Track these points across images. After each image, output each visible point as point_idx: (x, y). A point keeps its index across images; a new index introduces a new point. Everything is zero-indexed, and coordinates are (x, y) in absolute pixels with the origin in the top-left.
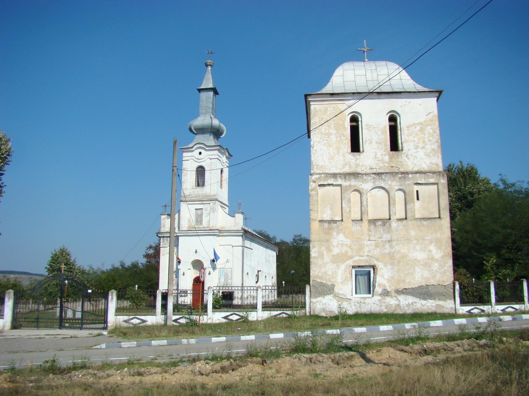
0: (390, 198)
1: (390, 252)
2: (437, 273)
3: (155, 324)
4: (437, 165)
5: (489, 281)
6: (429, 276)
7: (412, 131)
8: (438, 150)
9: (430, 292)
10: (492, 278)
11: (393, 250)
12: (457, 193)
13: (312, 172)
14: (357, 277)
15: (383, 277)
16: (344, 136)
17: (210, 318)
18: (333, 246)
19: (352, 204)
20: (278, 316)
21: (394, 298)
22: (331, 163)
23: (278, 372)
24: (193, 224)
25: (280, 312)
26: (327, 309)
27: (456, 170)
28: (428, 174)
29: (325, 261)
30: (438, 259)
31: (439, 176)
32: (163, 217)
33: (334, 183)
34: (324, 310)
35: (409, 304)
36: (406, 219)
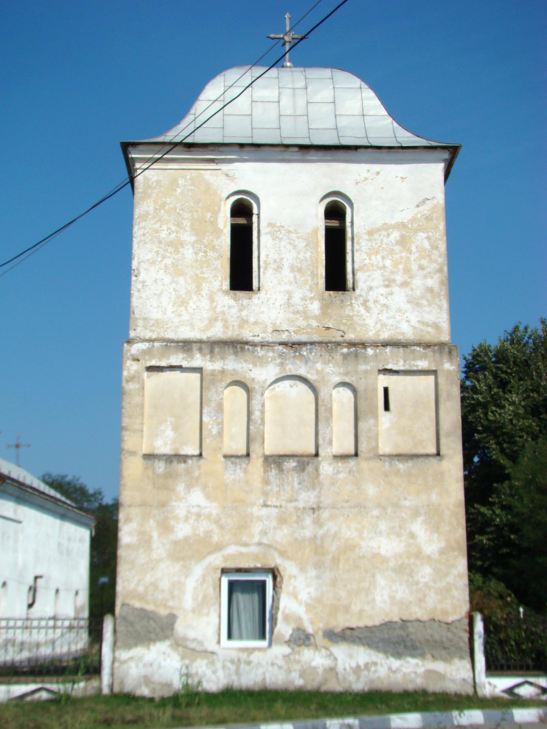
0: (320, 403)
1: (315, 536)
2: (430, 590)
4: (437, 327)
6: (410, 599)
7: (379, 242)
8: (441, 290)
9: (412, 640)
11: (321, 532)
12: (528, 397)
13: (132, 334)
14: (234, 596)
16: (214, 249)
18: (176, 518)
19: (226, 417)
21: (323, 652)
22: (180, 315)
25: (32, 687)
26: (156, 678)
27: (531, 341)
28: (413, 348)
29: (154, 555)
30: (433, 556)
31: (441, 353)
33: (185, 364)
34: (147, 680)
35: (358, 667)
36: (356, 455)
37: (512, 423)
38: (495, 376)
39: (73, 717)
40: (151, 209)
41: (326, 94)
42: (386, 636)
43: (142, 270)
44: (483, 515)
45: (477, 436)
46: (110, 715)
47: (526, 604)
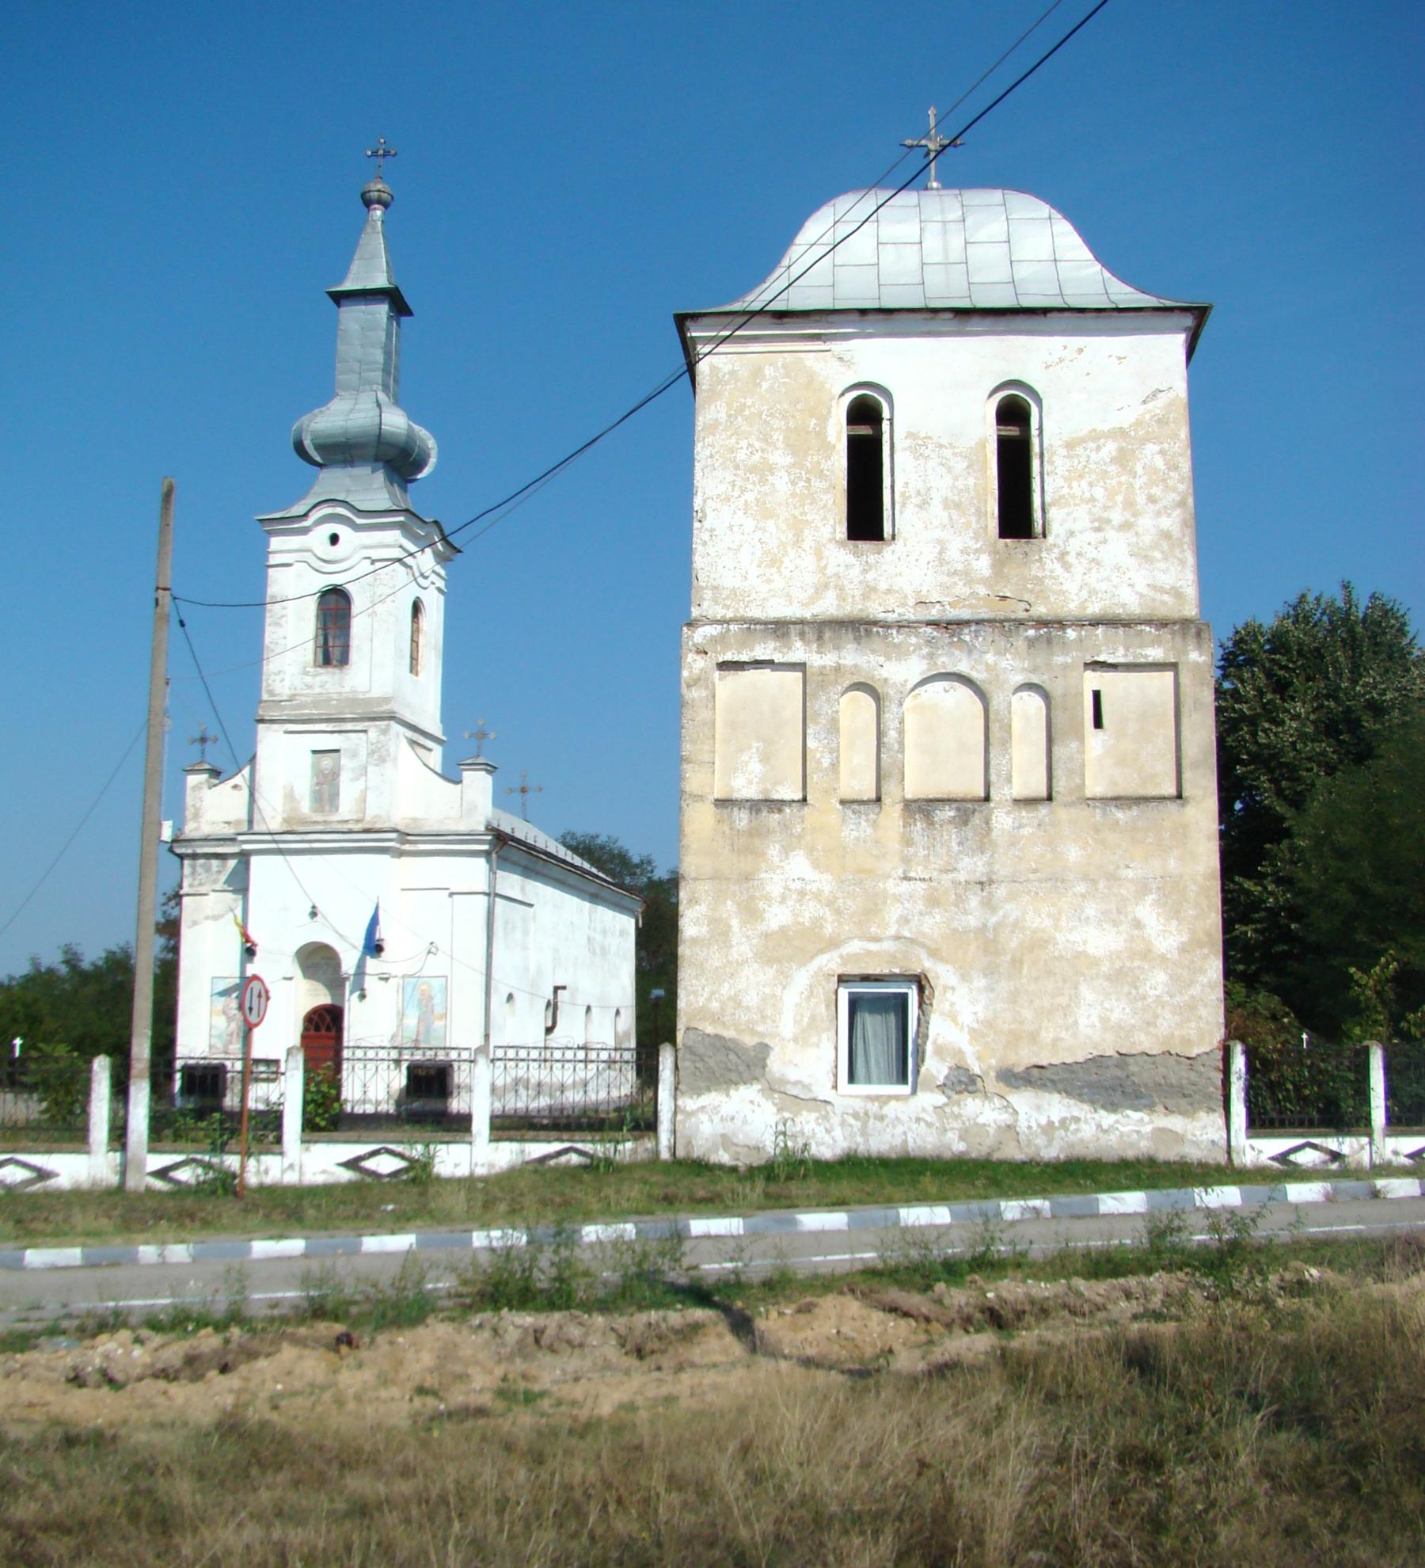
0: (992, 716)
1: (985, 925)
3: (86, 1186)
4: (1177, 593)
5: (1366, 1043)
7: (1083, 459)
10: (1379, 1034)
11: (993, 920)
13: (695, 612)
14: (858, 1018)
15: (954, 1019)
16: (821, 475)
17: (291, 1166)
18: (768, 899)
20: (552, 1162)
21: (996, 1100)
22: (769, 581)
23: (384, 1381)
24: (305, 807)
25: (557, 1146)
26: (740, 1138)
27: (1325, 618)
28: (1139, 627)
29: (734, 955)
31: (1184, 635)
32: (192, 780)
33: (778, 658)
34: (726, 1141)
35: (1050, 1123)
36: (1050, 798)
37: (1295, 749)
38: (1269, 674)
39: (618, 1192)
40: (722, 416)
41: (995, 228)
42: (1094, 1078)
43: (708, 511)
44: (1248, 893)
45: (1239, 770)
46: (672, 1190)
47: (1313, 1029)
